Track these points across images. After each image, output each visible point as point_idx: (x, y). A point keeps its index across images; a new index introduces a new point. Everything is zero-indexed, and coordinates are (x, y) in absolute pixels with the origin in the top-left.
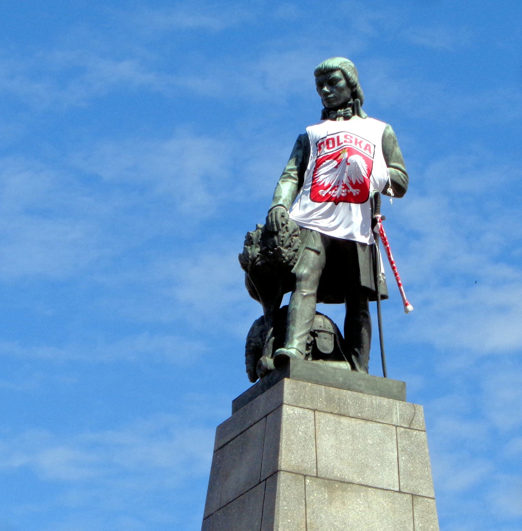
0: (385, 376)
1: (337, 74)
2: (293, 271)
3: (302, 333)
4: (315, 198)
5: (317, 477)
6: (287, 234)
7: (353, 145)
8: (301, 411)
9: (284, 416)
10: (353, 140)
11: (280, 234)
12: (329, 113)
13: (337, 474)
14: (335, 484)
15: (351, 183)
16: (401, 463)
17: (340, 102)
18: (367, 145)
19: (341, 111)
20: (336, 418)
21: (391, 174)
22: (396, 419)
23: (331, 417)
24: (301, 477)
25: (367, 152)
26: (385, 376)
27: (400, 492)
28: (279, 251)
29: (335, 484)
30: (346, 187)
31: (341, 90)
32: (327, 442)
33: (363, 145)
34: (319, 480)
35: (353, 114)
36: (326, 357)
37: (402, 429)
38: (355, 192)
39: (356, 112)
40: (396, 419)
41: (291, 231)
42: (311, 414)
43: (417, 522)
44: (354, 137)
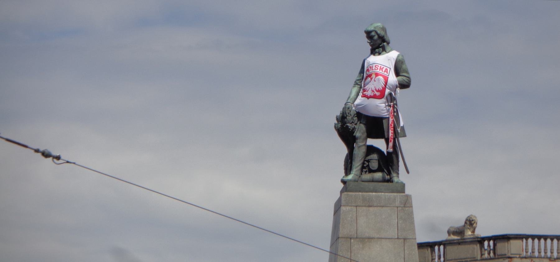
0: (408, 172)
1: (373, 34)
2: (354, 134)
3: (358, 164)
4: (364, 96)
5: (357, 238)
6: (350, 118)
7: (378, 71)
8: (350, 208)
9: (342, 212)
10: (379, 68)
11: (348, 118)
12: (373, 52)
13: (367, 235)
14: (365, 240)
15: (376, 90)
16: (399, 225)
17: (377, 46)
18: (386, 69)
19: (377, 50)
20: (367, 208)
21: (399, 81)
22: (397, 203)
23: (365, 208)
24: (349, 239)
25: (386, 73)
26: (408, 172)
27: (398, 238)
28: (347, 126)
29: (365, 240)
30: (373, 91)
31: (376, 41)
32: (362, 221)
33: (384, 70)
34: (358, 240)
35: (383, 51)
36: (374, 171)
37: (400, 208)
38: (378, 94)
39: (384, 50)
40: (397, 203)
41: (352, 115)
42: (355, 208)
43: (406, 251)
44: (380, 66)
